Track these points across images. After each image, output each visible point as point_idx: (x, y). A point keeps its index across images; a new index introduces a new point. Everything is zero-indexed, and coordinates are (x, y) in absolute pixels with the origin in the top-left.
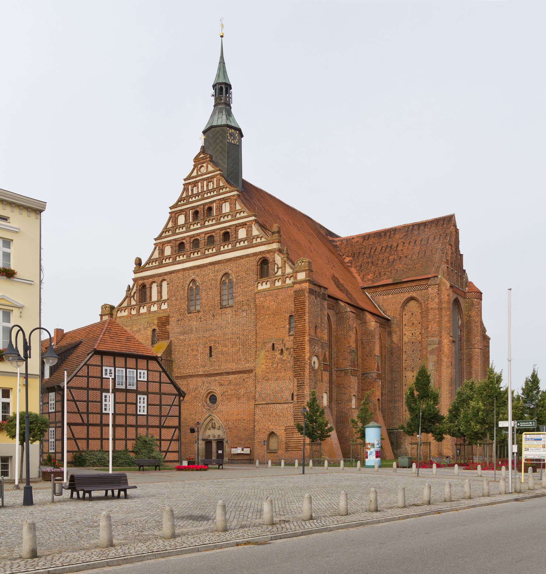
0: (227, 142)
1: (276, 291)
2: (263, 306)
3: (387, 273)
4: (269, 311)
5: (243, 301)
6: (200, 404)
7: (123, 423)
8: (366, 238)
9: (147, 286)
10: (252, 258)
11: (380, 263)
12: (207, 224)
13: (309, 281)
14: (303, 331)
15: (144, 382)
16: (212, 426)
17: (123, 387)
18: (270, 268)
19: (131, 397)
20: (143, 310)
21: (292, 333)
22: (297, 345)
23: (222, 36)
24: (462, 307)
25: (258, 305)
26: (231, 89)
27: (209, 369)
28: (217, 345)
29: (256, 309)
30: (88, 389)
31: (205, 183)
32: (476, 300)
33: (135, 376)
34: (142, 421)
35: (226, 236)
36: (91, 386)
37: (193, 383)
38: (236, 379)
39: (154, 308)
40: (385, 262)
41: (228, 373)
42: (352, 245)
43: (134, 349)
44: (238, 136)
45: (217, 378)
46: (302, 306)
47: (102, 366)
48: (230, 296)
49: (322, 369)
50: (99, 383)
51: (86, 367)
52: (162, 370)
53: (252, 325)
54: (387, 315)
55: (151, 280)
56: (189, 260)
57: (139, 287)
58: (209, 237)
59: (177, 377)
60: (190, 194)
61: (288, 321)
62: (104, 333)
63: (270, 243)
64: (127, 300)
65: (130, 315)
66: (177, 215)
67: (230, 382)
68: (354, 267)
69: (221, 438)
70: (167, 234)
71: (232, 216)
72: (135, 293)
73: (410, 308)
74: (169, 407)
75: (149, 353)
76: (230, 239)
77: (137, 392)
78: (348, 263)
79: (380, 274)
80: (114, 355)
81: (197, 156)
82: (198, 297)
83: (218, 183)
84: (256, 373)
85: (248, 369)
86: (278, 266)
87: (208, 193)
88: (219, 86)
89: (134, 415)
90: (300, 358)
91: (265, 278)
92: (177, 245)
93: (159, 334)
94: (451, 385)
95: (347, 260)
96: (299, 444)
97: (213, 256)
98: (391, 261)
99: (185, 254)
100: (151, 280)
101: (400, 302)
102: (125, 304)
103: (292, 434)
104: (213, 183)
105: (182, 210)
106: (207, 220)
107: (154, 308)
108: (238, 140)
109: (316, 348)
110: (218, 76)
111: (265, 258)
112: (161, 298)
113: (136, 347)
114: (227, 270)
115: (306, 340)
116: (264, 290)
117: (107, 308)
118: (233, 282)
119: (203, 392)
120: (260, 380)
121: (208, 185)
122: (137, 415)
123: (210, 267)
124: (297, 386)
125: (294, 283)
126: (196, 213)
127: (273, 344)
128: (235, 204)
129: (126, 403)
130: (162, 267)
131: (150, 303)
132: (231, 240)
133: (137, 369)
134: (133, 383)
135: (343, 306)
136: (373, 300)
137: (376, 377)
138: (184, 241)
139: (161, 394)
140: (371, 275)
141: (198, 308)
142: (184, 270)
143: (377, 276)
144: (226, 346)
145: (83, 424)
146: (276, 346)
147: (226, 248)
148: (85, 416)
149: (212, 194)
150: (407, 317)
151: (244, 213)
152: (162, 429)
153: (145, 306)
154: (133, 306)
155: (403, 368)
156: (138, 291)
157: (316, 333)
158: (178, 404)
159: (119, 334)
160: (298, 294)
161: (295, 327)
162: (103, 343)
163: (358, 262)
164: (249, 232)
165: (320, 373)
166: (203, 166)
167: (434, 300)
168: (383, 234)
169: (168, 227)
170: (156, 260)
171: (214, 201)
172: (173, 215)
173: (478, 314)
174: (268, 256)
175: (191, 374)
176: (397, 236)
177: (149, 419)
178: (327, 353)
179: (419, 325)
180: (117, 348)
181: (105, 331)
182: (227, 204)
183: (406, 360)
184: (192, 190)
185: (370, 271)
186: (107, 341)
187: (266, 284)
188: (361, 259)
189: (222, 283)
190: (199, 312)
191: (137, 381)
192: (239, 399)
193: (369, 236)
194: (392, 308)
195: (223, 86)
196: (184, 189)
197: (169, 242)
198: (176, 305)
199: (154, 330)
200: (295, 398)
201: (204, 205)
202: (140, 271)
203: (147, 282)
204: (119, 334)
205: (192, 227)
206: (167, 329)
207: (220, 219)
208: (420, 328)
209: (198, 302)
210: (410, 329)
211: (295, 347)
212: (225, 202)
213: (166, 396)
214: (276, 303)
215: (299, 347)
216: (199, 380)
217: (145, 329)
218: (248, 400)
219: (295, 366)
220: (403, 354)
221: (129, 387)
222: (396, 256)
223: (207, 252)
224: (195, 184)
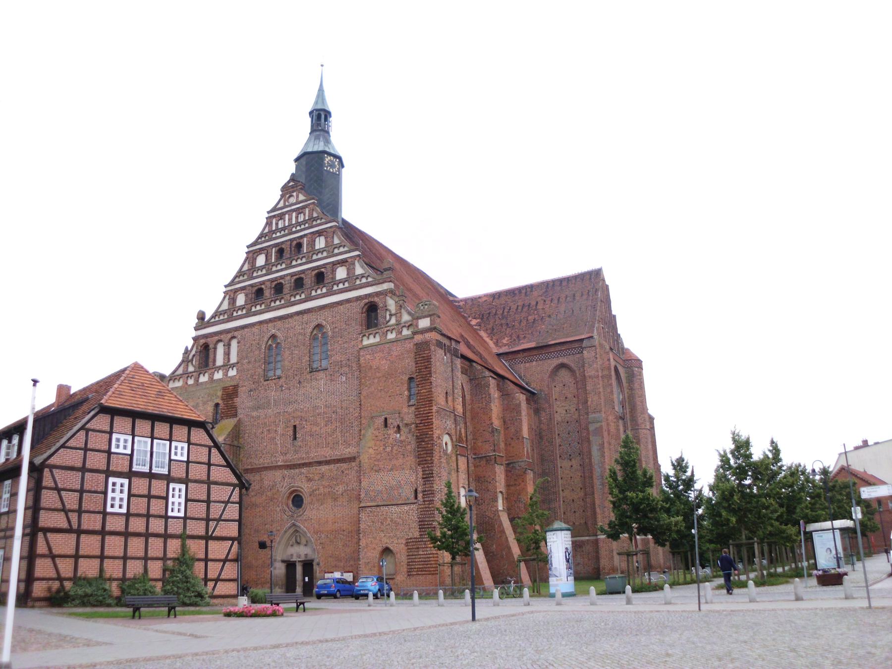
1: (388, 346)
2: (371, 366)
3: (528, 336)
4: (379, 372)
5: (341, 361)
6: (278, 509)
7: (142, 529)
8: (497, 297)
9: (210, 346)
10: (354, 304)
11: (516, 324)
12: (294, 263)
15: (182, 463)
16: (296, 541)
17: (146, 469)
18: (379, 316)
19: (158, 487)
20: (203, 379)
21: (412, 402)
22: (421, 419)
23: (322, 66)
26: (330, 116)
29: (360, 371)
30: (83, 469)
31: (294, 214)
33: (168, 451)
34: (175, 528)
35: (320, 277)
36: (89, 465)
37: (269, 478)
38: (331, 470)
39: (218, 375)
40: (524, 323)
41: (320, 463)
42: (479, 305)
43: (167, 408)
44: (339, 164)
45: (304, 470)
46: (426, 364)
47: (111, 433)
48: (324, 356)
50: (105, 461)
51: (83, 433)
52: (213, 444)
53: (355, 393)
55: (217, 338)
56: (269, 309)
57: (199, 348)
58: (296, 280)
59: (247, 471)
60: (274, 228)
61: (406, 385)
62: (122, 382)
63: (379, 284)
64: (182, 366)
65: (186, 386)
66: (255, 255)
67: (323, 476)
69: (309, 558)
70: (241, 278)
71: (328, 252)
72: (194, 356)
74: (222, 504)
75: (192, 416)
76: (325, 281)
77: (168, 479)
78: (475, 325)
80: (134, 415)
81: (286, 184)
82: (279, 358)
83: (311, 214)
84: (360, 461)
85: (349, 456)
87: (297, 226)
88: (317, 113)
89: (160, 517)
90: (426, 437)
91: (372, 329)
92: (254, 291)
95: (474, 322)
96: (427, 564)
99: (263, 303)
100: (217, 338)
101: (548, 370)
103: (416, 550)
104: (304, 215)
105: (262, 248)
106: (294, 259)
107: (218, 375)
108: (339, 169)
109: (448, 422)
110: (316, 103)
111: (373, 303)
112: (229, 361)
113: (172, 405)
114: (319, 321)
116: (371, 345)
118: (328, 336)
119: (284, 489)
120: (367, 471)
121: (298, 217)
122: (166, 517)
123: (296, 318)
125: (414, 333)
126: (281, 252)
127: (386, 419)
129: (149, 497)
130: (232, 321)
131: (213, 368)
132: (326, 281)
133: (170, 440)
134: (163, 463)
135: (479, 370)
137: (526, 467)
138: (263, 286)
139: (209, 483)
140: (506, 339)
141: (279, 372)
142: (261, 323)
143: (515, 340)
144: (317, 424)
145: (69, 531)
147: (319, 292)
148: (74, 517)
149: (303, 227)
150: (557, 389)
152: (211, 543)
153: (206, 372)
154: (190, 373)
155: (557, 456)
156: (198, 354)
157: (447, 401)
158: (237, 500)
159: (146, 385)
161: (418, 393)
162: (116, 396)
163: (489, 324)
164: (351, 271)
165: (454, 458)
169: (243, 270)
170: (225, 312)
171: (305, 235)
172: (251, 255)
174: (376, 299)
175: (266, 465)
177: (188, 525)
178: (463, 431)
180: (139, 405)
181: (125, 380)
182: (322, 239)
183: (560, 445)
184: (277, 224)
185: (505, 334)
186: (123, 393)
187: (375, 337)
188: (492, 321)
189: (314, 338)
190: (279, 378)
191: (170, 460)
192: (335, 500)
194: (538, 378)
196: (267, 223)
198: (249, 370)
199: (217, 405)
200: (420, 496)
202: (203, 326)
203: (211, 341)
204: (146, 385)
205: (274, 269)
207: (312, 257)
208: (576, 402)
209: (279, 365)
210: (563, 404)
211: (418, 422)
212: (319, 236)
213: (218, 486)
214: (388, 362)
215: (424, 422)
216: (278, 474)
217: (205, 403)
218: (349, 501)
219: (419, 450)
221: (155, 470)
222: (536, 316)
223: (293, 299)
224: (281, 217)
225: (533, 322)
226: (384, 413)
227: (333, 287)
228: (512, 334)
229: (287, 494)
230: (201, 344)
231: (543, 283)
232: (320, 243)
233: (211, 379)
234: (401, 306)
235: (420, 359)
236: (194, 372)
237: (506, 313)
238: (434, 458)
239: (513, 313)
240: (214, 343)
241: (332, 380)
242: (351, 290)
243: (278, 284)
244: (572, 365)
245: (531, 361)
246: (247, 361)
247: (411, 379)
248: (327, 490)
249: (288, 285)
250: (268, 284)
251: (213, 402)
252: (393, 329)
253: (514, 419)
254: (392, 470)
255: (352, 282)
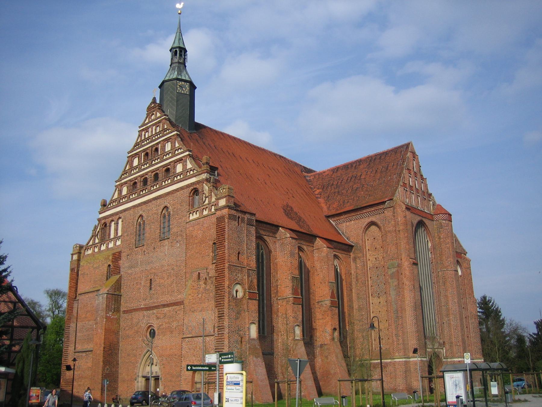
0: (177, 92)
2: (192, 235)
3: (350, 201)
4: (196, 240)
10: (185, 190)
13: (228, 206)
14: (223, 258)
20: (103, 248)
24: (430, 229)
25: (188, 235)
27: (150, 302)
28: (156, 277)
32: (444, 221)
38: (170, 311)
39: (111, 245)
41: (164, 306)
42: (323, 178)
46: (222, 232)
49: (248, 297)
54: (351, 241)
56: (140, 197)
60: (143, 139)
64: (92, 239)
68: (322, 198)
69: (157, 375)
73: (371, 233)
78: (317, 194)
79: (344, 202)
81: (149, 106)
86: (205, 195)
87: (155, 136)
92: (131, 184)
93: (113, 269)
94: (415, 310)
97: (156, 192)
98: (354, 189)
99: (136, 193)
102: (91, 243)
104: (160, 127)
107: (111, 245)
111: (196, 189)
112: (117, 233)
115: (226, 267)
117: (77, 248)
119: (144, 325)
121: (156, 129)
123: (153, 202)
124: (219, 317)
126: (147, 154)
128: (175, 142)
131: (108, 240)
136: (337, 227)
138: (136, 181)
142: (134, 207)
144: (163, 278)
146: (201, 275)
151: (181, 150)
160: (220, 220)
164: (185, 166)
166: (153, 114)
167: (390, 223)
168: (349, 166)
171: (160, 142)
172: (130, 158)
173: (448, 235)
174: (197, 186)
175: (135, 308)
176: (362, 167)
179: (382, 249)
182: (169, 143)
184: (145, 135)
185: (336, 200)
188: (329, 189)
192: (172, 332)
193: (338, 169)
195: (178, 50)
196: (139, 135)
197: (126, 183)
199: (109, 266)
201: (152, 146)
206: (119, 264)
212: (168, 142)
216: (141, 313)
217: (103, 265)
220: (368, 280)
224: (146, 130)
225: (356, 190)
226: (198, 270)
227: (174, 179)
228: (340, 200)
229: (146, 329)
230: (103, 223)
231: (368, 158)
232: (168, 147)
233: (107, 247)
234: (211, 191)
235: (219, 229)
236: (98, 243)
237: (339, 184)
238: (225, 302)
239: (344, 183)
240: (109, 222)
241: (172, 246)
242: (183, 181)
243: (145, 178)
244: (379, 223)
245: (350, 221)
246: (126, 234)
247: (214, 243)
248: (167, 325)
249: (150, 179)
250: (139, 178)
251: (107, 264)
252: (207, 208)
253: (323, 267)
254: (201, 311)
255: (185, 173)
